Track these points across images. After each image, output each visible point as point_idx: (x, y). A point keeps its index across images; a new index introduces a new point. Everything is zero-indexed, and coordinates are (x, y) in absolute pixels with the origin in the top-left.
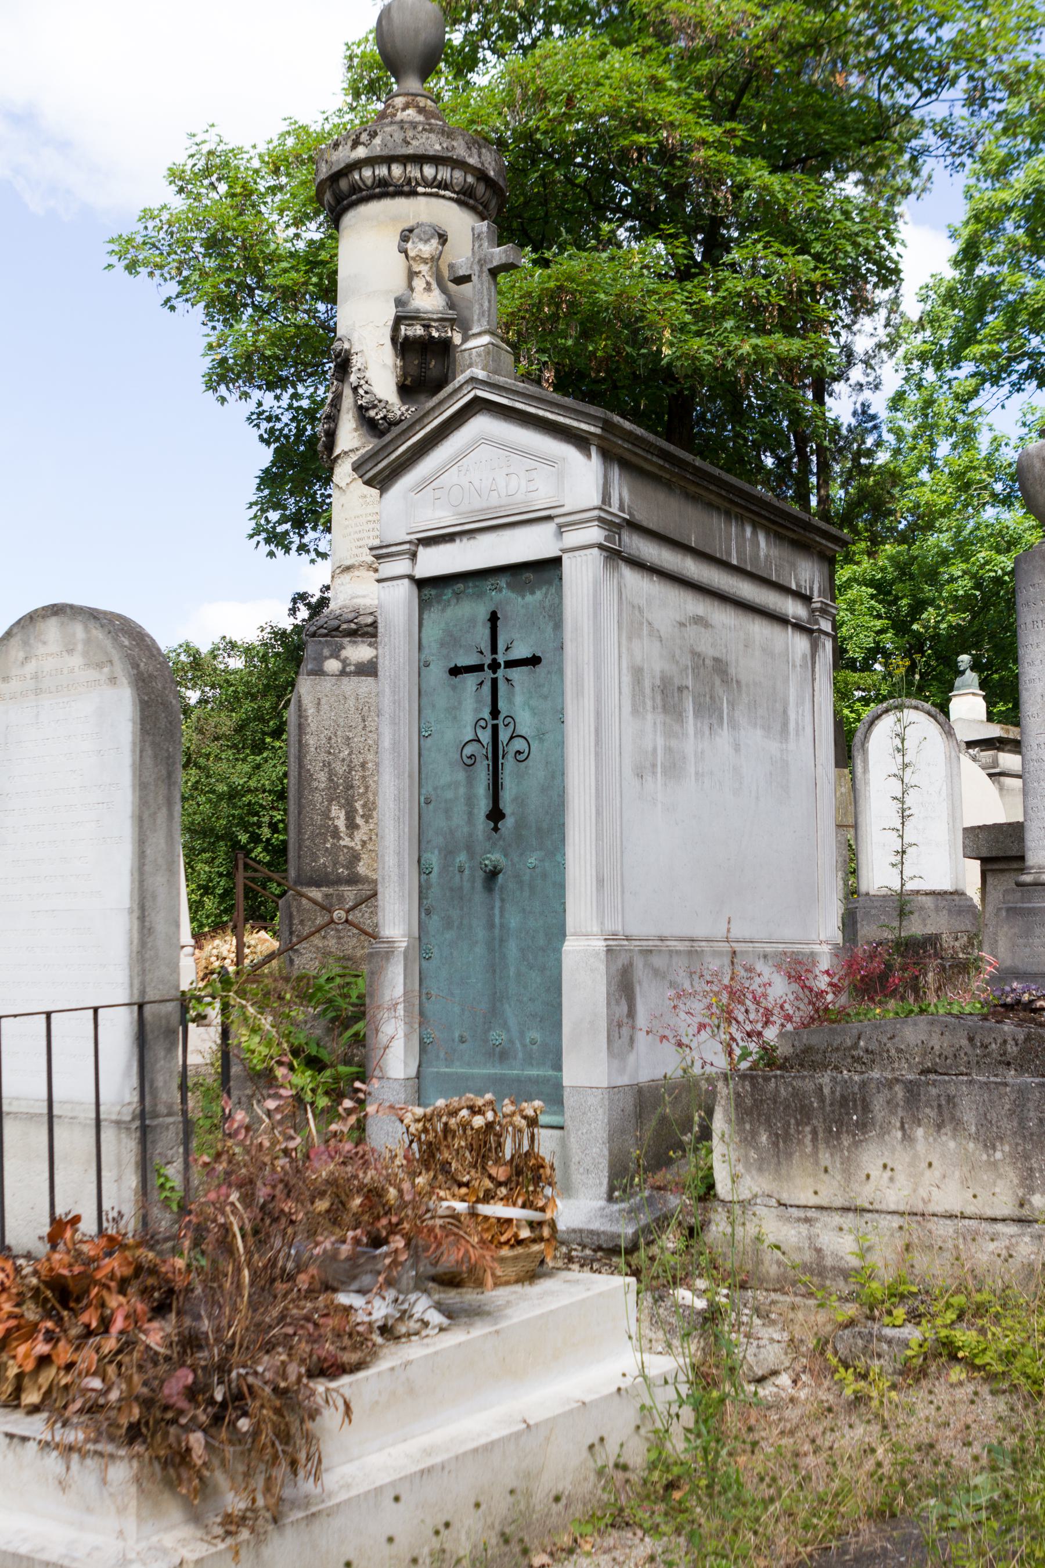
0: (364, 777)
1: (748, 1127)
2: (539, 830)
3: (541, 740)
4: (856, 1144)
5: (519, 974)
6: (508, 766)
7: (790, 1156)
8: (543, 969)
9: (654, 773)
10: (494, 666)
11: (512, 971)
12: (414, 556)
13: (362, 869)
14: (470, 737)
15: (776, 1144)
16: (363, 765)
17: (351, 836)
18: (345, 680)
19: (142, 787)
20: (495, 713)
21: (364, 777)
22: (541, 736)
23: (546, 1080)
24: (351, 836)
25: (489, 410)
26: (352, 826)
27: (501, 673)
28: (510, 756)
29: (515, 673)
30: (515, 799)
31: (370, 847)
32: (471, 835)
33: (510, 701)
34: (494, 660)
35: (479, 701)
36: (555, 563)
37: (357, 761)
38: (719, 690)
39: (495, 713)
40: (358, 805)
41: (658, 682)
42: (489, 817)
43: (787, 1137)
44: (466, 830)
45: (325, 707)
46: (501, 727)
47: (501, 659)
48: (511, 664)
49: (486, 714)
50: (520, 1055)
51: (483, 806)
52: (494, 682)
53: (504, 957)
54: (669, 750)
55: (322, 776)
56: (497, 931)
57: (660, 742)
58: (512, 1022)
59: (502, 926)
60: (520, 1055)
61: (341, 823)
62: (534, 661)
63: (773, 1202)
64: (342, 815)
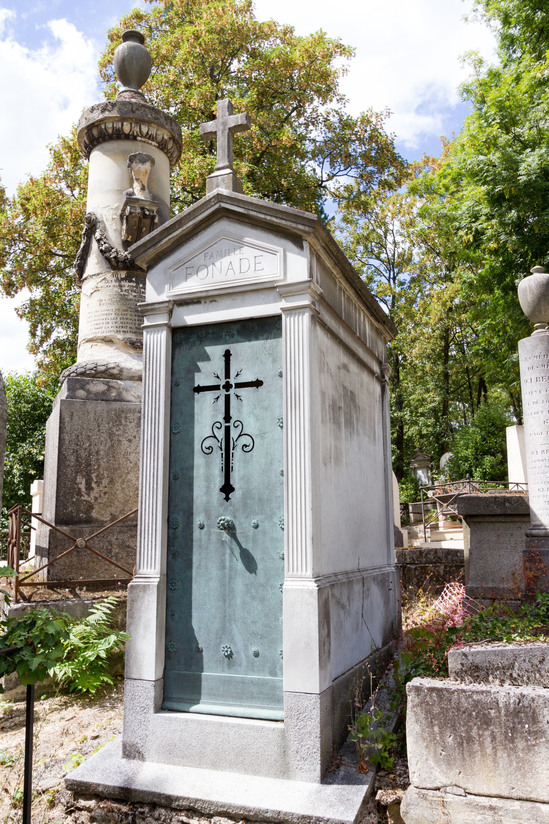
0: (97, 460)
1: (436, 729)
2: (260, 500)
3: (262, 438)
4: (529, 748)
5: (244, 603)
6: (237, 455)
7: (472, 754)
8: (263, 600)
9: (331, 462)
10: (228, 386)
11: (239, 601)
12: (171, 313)
13: (94, 514)
14: (210, 434)
15: (461, 744)
16: (97, 452)
17: (89, 495)
18: (88, 403)
19: (506, 448)
20: (227, 418)
21: (97, 460)
22: (262, 435)
23: (264, 683)
24: (89, 495)
25: (228, 217)
26: (89, 488)
27: (232, 391)
28: (239, 449)
29: (242, 392)
30: (243, 478)
31: (99, 501)
32: (208, 502)
33: (239, 411)
34: (227, 383)
35: (216, 410)
36: (278, 318)
37: (94, 449)
38: (353, 411)
39: (227, 418)
40: (93, 476)
41: (331, 403)
42: (222, 490)
43: (470, 740)
44: (204, 498)
45: (76, 418)
46: (232, 428)
47: (232, 381)
48: (239, 385)
49: (221, 417)
50: (244, 663)
51: (219, 481)
52: (227, 398)
53: (232, 591)
54: (336, 447)
55: (73, 458)
56: (227, 571)
57: (333, 443)
58: (238, 638)
59: (231, 567)
60: (244, 663)
61: (83, 487)
62: (258, 384)
63: (462, 792)
64: (84, 482)
